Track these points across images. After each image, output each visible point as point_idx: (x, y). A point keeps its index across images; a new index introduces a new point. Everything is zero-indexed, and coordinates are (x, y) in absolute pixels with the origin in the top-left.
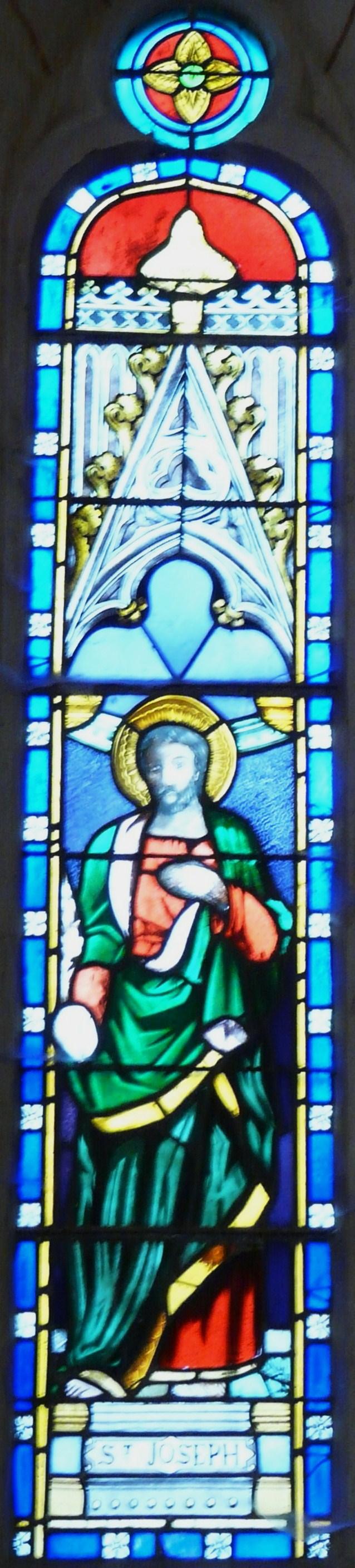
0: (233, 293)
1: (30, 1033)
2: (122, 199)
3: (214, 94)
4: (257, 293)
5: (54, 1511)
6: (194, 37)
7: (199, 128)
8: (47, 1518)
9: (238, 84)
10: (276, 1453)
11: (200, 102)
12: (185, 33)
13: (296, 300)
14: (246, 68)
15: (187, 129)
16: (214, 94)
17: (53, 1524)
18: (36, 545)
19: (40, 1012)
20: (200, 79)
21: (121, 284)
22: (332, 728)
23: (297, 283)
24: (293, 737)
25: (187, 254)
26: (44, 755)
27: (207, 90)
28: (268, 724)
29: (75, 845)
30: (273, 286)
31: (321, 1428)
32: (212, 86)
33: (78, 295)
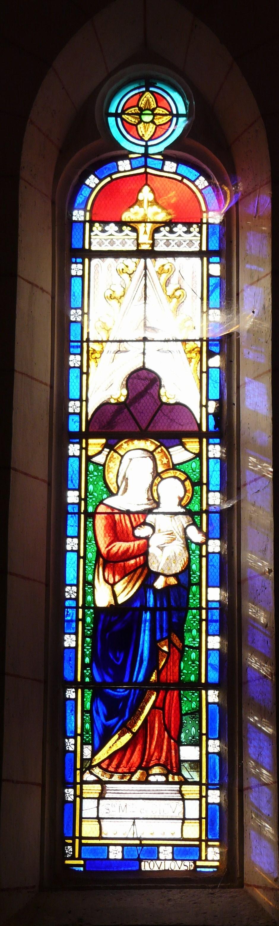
0: (167, 229)
1: (76, 222)
2: (112, 180)
3: (157, 126)
4: (180, 229)
5: (84, 835)
6: (148, 95)
7: (150, 143)
8: (81, 838)
9: (171, 120)
10: (193, 809)
11: (150, 130)
12: (143, 93)
13: (200, 232)
14: (175, 112)
15: (144, 143)
16: (157, 126)
17: (84, 841)
18: (69, 534)
19: (79, 312)
20: (150, 118)
21: (112, 225)
22: (221, 357)
23: (200, 224)
24: (199, 455)
25: (146, 209)
26: (77, 418)
27: (154, 123)
28: (186, 449)
29: (90, 509)
30: (188, 225)
31: (215, 796)
32: (157, 122)
33: (91, 231)
